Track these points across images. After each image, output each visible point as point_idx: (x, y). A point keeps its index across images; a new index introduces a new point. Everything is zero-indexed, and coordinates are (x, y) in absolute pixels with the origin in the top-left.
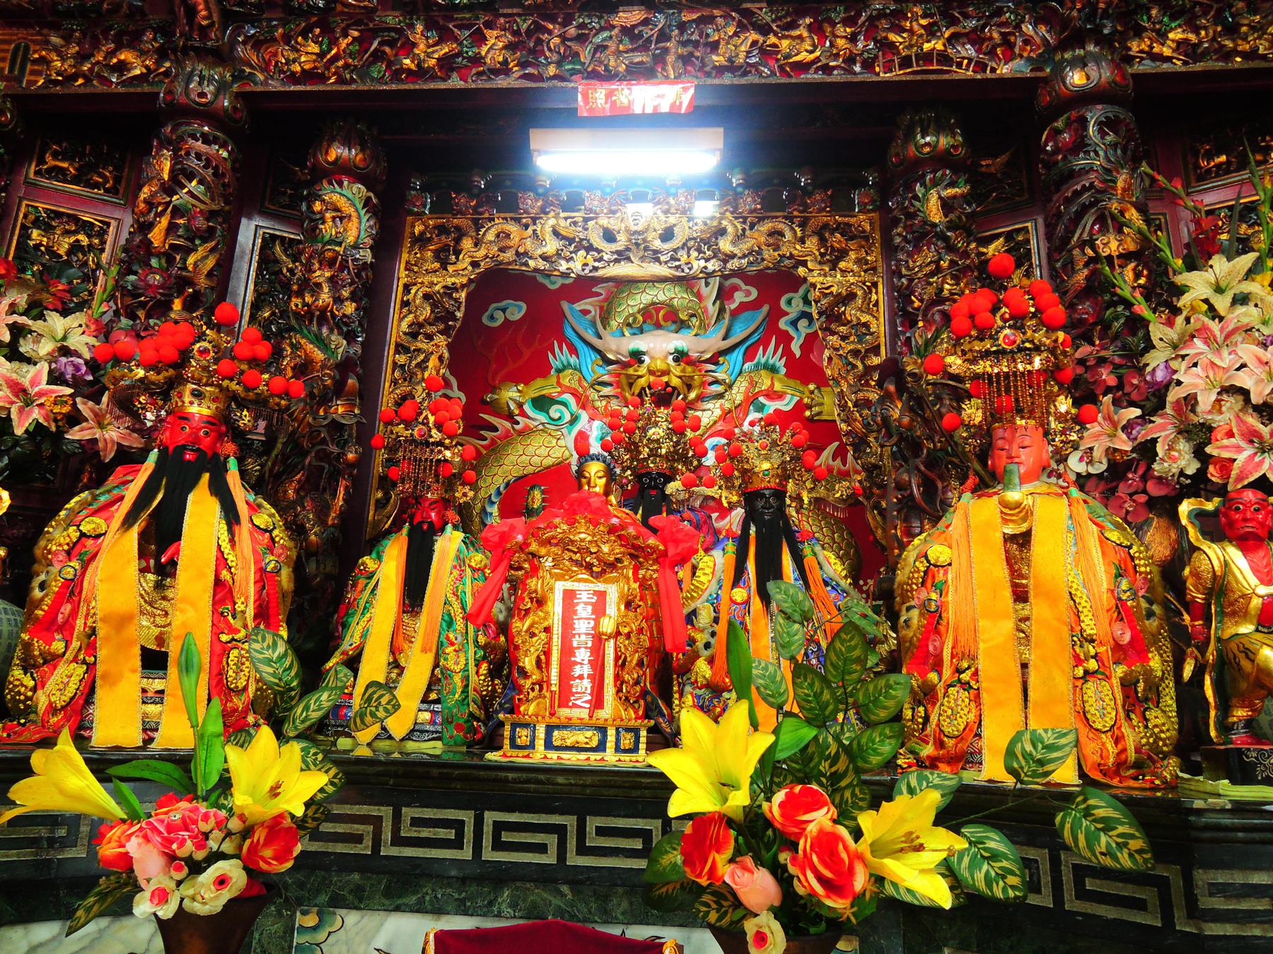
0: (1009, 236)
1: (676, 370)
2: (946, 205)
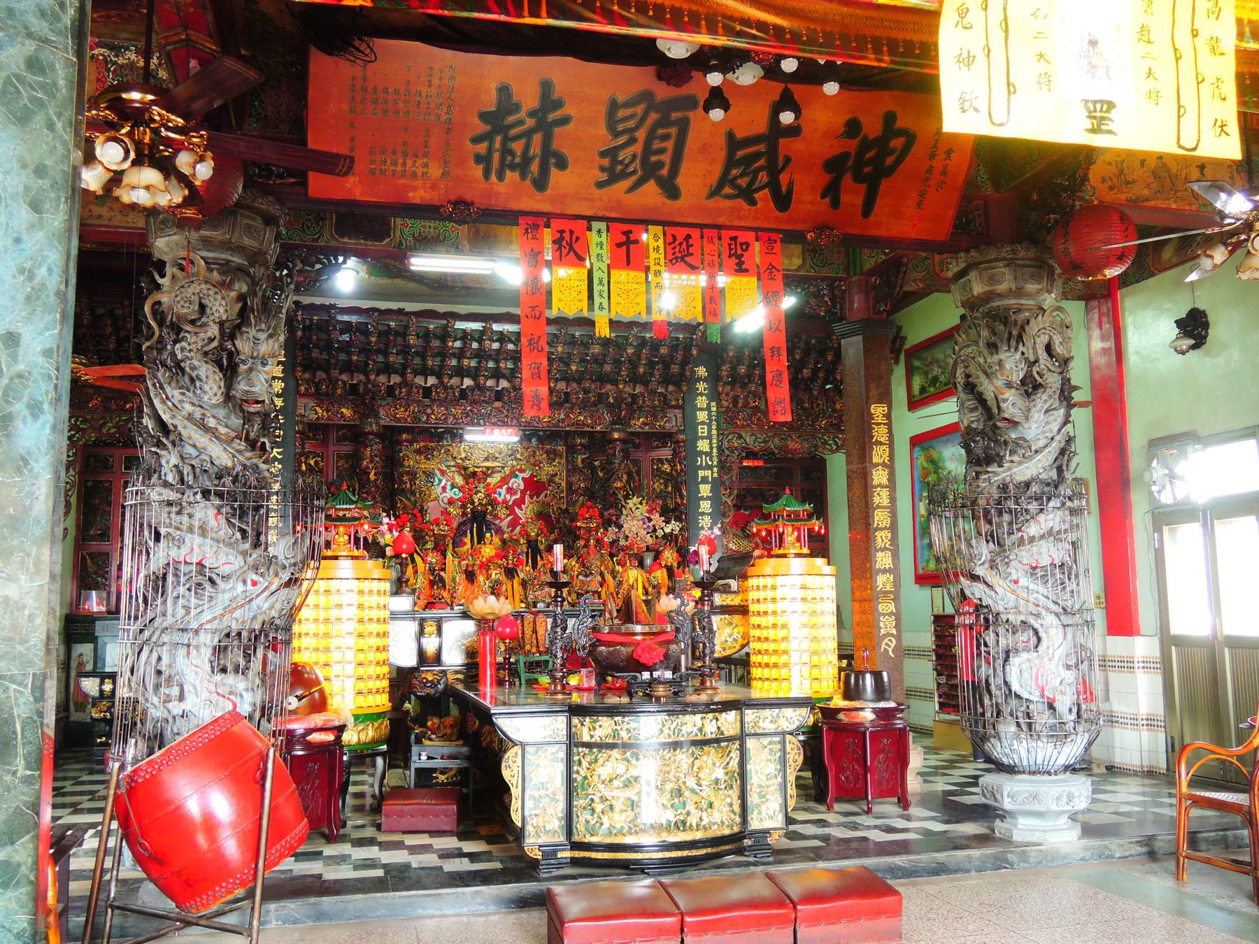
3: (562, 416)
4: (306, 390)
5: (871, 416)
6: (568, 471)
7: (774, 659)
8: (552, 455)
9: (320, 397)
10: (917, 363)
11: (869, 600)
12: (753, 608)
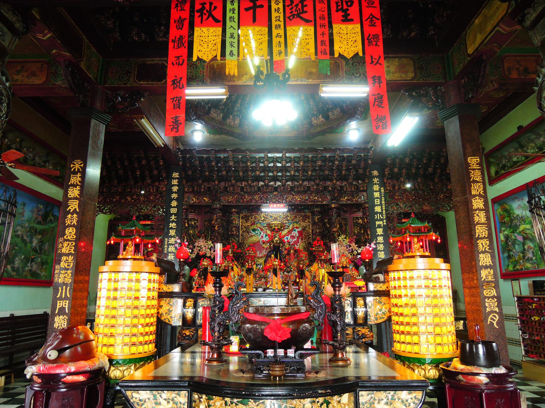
3: (307, 198)
4: (188, 190)
5: (468, 165)
7: (408, 329)
8: (305, 218)
9: (197, 194)
10: (492, 160)
11: (477, 287)
12: (393, 292)
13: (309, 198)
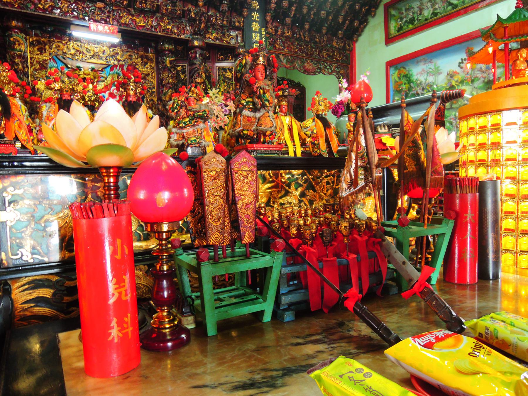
0: (182, 66)
1: (92, 74)
2: (171, 62)
3: (154, 24)
6: (158, 69)
10: (393, 12)
13: (159, 24)
